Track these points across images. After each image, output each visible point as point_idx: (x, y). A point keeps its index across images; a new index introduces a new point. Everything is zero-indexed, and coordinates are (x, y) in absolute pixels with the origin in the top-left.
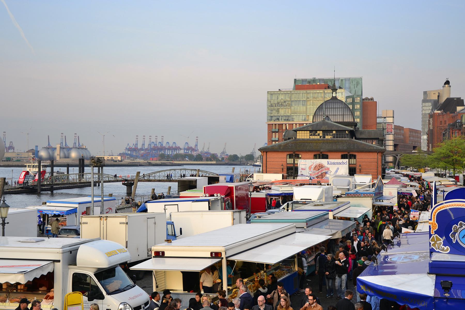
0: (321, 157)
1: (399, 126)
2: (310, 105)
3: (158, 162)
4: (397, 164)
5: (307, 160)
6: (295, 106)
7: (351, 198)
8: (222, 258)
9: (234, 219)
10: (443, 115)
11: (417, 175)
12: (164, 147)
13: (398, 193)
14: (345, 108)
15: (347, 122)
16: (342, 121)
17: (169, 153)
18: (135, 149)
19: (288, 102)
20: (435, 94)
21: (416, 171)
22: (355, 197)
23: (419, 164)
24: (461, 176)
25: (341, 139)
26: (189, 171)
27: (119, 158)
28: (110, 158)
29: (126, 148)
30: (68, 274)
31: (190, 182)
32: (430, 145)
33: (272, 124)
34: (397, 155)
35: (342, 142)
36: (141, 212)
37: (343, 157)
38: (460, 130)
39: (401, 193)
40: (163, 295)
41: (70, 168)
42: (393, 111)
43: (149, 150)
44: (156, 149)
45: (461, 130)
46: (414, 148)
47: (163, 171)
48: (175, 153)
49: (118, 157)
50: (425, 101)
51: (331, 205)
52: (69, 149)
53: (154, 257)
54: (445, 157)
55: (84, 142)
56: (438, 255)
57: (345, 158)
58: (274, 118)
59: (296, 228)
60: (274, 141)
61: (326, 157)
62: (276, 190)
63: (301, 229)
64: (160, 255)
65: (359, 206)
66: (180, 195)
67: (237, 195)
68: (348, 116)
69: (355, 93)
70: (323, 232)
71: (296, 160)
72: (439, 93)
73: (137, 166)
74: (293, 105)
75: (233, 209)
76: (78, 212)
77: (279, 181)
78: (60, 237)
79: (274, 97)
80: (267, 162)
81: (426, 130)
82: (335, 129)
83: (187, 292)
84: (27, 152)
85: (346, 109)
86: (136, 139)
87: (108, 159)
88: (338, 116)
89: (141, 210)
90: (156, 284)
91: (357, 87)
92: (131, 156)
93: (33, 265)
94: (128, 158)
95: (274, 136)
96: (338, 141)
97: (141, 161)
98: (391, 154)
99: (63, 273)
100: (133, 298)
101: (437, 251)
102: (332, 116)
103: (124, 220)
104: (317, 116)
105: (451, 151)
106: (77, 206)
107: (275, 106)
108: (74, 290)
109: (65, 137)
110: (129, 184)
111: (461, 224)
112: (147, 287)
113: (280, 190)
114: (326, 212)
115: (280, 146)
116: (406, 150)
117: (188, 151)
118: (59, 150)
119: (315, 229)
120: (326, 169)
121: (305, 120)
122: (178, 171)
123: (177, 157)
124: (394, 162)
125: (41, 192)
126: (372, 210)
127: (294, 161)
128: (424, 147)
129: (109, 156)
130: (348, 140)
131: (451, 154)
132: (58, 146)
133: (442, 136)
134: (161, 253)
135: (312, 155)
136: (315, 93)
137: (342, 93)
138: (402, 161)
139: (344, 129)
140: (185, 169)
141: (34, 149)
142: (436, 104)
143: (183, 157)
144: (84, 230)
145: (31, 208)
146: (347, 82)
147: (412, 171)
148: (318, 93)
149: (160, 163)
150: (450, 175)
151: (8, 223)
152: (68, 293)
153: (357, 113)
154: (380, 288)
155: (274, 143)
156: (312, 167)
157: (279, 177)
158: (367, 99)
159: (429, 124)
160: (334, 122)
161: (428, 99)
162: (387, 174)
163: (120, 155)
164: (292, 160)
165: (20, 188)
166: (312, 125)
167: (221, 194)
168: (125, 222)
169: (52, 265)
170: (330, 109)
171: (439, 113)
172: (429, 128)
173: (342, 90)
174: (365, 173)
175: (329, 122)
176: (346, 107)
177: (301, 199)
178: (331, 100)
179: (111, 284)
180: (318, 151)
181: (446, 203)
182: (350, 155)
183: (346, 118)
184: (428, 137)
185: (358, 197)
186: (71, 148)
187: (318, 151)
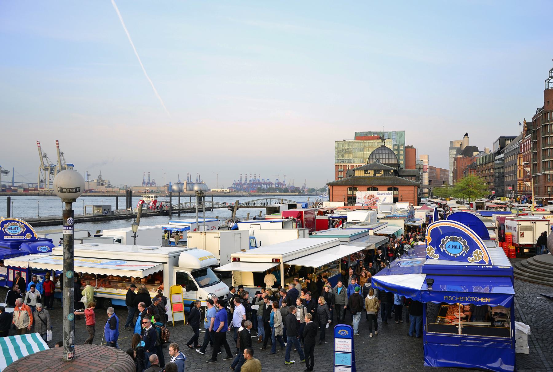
0: (373, 189)
2: (367, 151)
3: (256, 193)
4: (431, 195)
5: (363, 192)
6: (356, 152)
8: (281, 263)
9: (299, 235)
10: (464, 159)
11: (444, 202)
13: (426, 216)
14: (391, 153)
16: (389, 163)
17: (264, 187)
18: (240, 184)
19: (350, 149)
20: (458, 143)
22: (393, 219)
23: (445, 194)
24: (474, 203)
25: (387, 176)
26: (276, 200)
27: (228, 191)
28: (221, 190)
29: (233, 183)
31: (275, 208)
32: (455, 180)
33: (339, 165)
34: (431, 188)
35: (388, 178)
36: (234, 229)
37: (389, 189)
38: (476, 170)
39: (429, 216)
40: (238, 289)
42: (428, 155)
43: (249, 185)
44: (255, 184)
45: (477, 170)
46: (444, 183)
47: (258, 200)
48: (269, 187)
50: (451, 148)
52: (193, 184)
53: (232, 262)
54: (462, 190)
55: (203, 179)
57: (390, 191)
59: (341, 241)
60: (340, 178)
61: (376, 190)
62: (337, 214)
63: (345, 243)
64: (236, 260)
65: (394, 225)
66: (266, 218)
67: (306, 217)
68: (394, 159)
69: (400, 142)
70: (362, 244)
71: (354, 191)
72: (461, 143)
74: (354, 151)
75: (303, 227)
76: (191, 229)
77: (341, 207)
78: (178, 247)
79: (340, 146)
80: (333, 194)
81: (452, 169)
82: (383, 169)
83: (256, 287)
84: (164, 186)
85: (392, 154)
86: (284, 178)
88: (386, 159)
89: (234, 228)
90: (234, 281)
91: (401, 138)
92: (237, 189)
93: (149, 266)
94: (234, 190)
96: (385, 178)
97: (244, 193)
99: (169, 271)
100: (218, 291)
101: (431, 257)
103: (217, 235)
104: (370, 159)
105: (468, 186)
106: (190, 225)
107: (341, 152)
108: (177, 283)
109: (190, 175)
111: (447, 238)
112: (229, 284)
114: (367, 230)
115: (342, 181)
116: (438, 184)
117: (278, 186)
118: (186, 185)
119: (356, 242)
120: (376, 199)
121: (363, 162)
122: (268, 200)
123: (270, 190)
124: (429, 193)
125: (172, 215)
126: (404, 228)
128: (451, 183)
130: (392, 177)
131: (467, 187)
132: (185, 182)
133: (463, 174)
134: (237, 259)
135: (366, 188)
136: (370, 142)
137: (390, 142)
138: (434, 192)
139: (390, 169)
141: (169, 184)
142: (460, 151)
143: (274, 190)
144: (190, 241)
145: (159, 226)
146: (394, 134)
147: (440, 200)
148: (372, 142)
149: (258, 194)
150: (467, 203)
151: (138, 236)
152: (173, 285)
153: (402, 157)
154: (389, 285)
155: (340, 179)
156: (366, 197)
157: (342, 204)
158: (408, 147)
159: (454, 165)
160: (383, 164)
161: (453, 146)
162: (422, 202)
163: (229, 188)
164: (352, 191)
166: (366, 166)
168: (218, 237)
169: (162, 265)
170: (381, 154)
171: (461, 157)
172: (454, 168)
173: (390, 140)
175: (379, 163)
176: (392, 153)
177: (353, 221)
178: (381, 148)
179: (203, 280)
180: (370, 185)
181: (437, 223)
183: (392, 161)
184: (453, 175)
185: (395, 219)
186: (195, 184)
187: (370, 185)
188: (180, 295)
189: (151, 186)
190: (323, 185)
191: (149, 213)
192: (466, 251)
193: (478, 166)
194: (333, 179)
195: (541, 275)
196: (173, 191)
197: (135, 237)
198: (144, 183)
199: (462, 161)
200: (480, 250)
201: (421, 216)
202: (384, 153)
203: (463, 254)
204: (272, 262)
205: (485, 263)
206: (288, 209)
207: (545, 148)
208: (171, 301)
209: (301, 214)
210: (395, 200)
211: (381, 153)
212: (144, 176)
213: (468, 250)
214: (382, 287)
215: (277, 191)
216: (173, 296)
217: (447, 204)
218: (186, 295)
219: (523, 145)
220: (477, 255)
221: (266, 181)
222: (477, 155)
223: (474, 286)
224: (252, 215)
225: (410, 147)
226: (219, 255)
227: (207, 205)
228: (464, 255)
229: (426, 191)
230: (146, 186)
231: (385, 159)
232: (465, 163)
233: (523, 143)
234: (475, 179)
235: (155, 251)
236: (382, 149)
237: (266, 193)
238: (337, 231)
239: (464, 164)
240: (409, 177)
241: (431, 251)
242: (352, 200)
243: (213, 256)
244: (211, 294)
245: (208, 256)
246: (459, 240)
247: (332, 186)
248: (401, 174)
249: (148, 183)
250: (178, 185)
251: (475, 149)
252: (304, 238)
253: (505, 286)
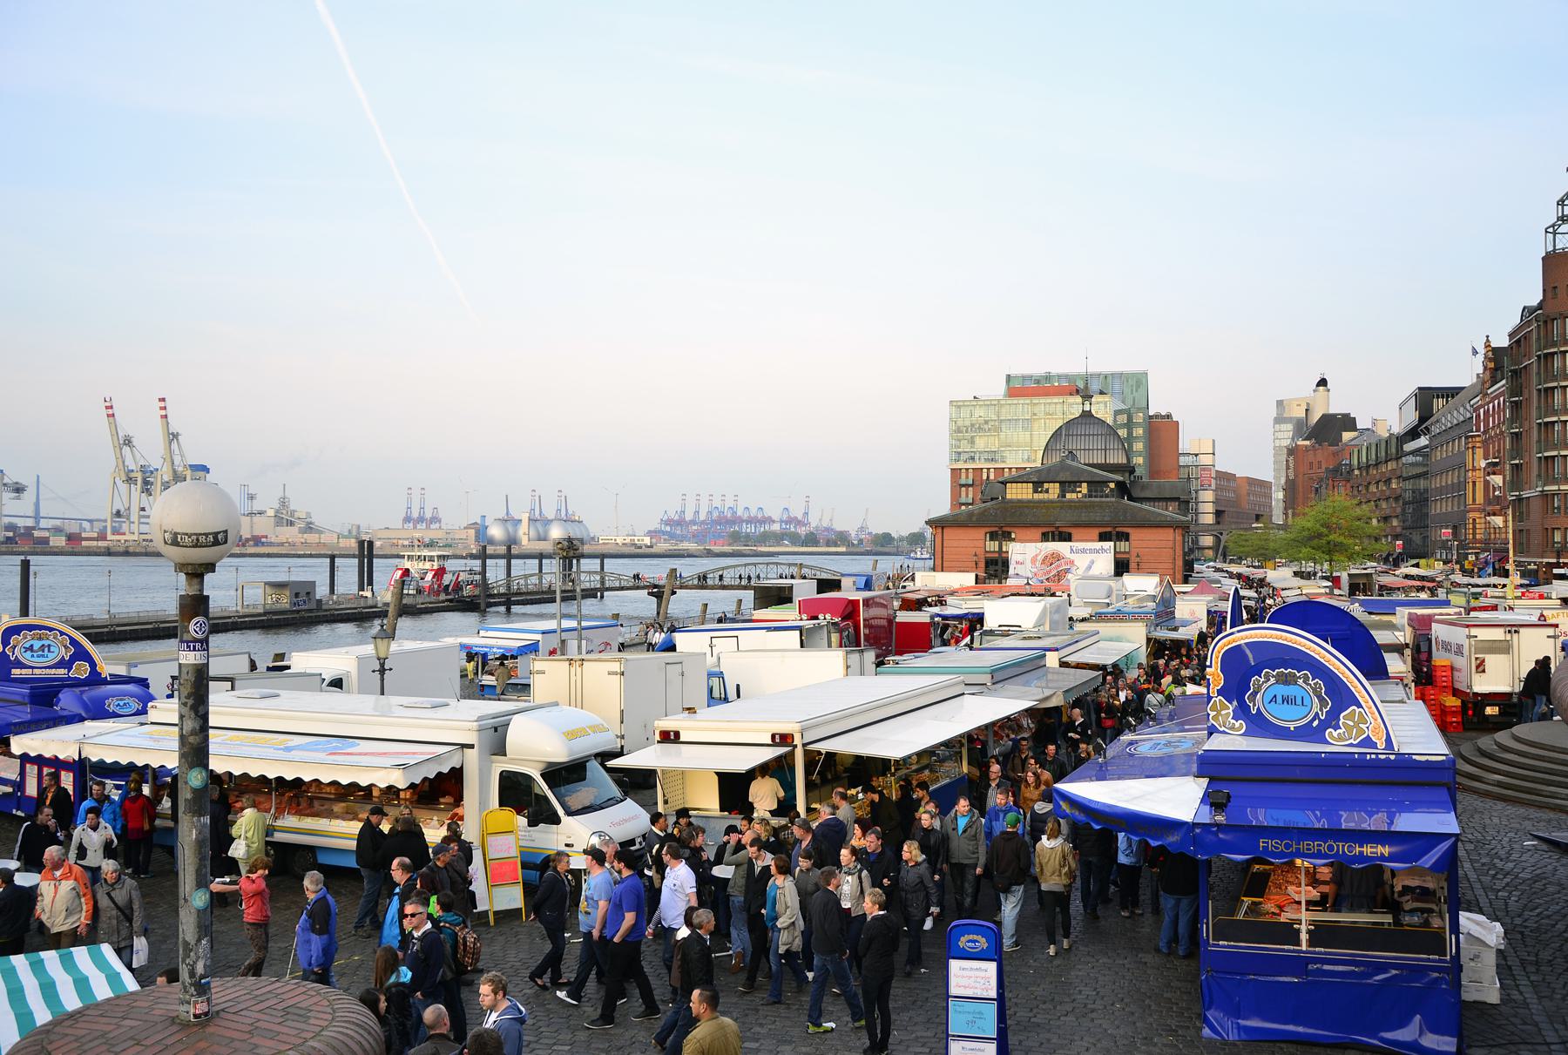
0: (1056, 537)
1: (1226, 473)
3: (727, 549)
4: (1222, 552)
7: (1119, 622)
8: (796, 746)
9: (848, 667)
11: (1258, 574)
12: (740, 517)
13: (1209, 612)
14: (1110, 435)
15: (1118, 464)
16: (1103, 462)
17: (748, 530)
18: (680, 523)
20: (1300, 405)
21: (1258, 567)
22: (1115, 620)
23: (1263, 551)
24: (1344, 576)
25: (1098, 499)
27: (647, 541)
29: (662, 520)
30: (490, 773)
31: (781, 589)
32: (1290, 512)
33: (960, 469)
34: (1221, 534)
35: (1100, 505)
37: (1104, 537)
39: (1215, 612)
40: (674, 819)
41: (544, 561)
42: (1214, 441)
43: (707, 524)
44: (723, 521)
45: (1351, 482)
46: (1258, 518)
47: (733, 569)
48: (762, 529)
49: (645, 538)
50: (1279, 420)
51: (1059, 637)
52: (547, 522)
53: (658, 742)
54: (1311, 538)
56: (1221, 738)
59: (966, 684)
60: (964, 504)
61: (1066, 537)
62: (955, 607)
63: (979, 688)
64: (669, 737)
65: (1118, 639)
66: (753, 618)
67: (867, 616)
68: (1116, 451)
69: (1134, 404)
70: (1025, 692)
71: (1004, 543)
72: (1308, 404)
73: (682, 556)
74: (1004, 429)
76: (540, 649)
78: (504, 700)
79: (965, 413)
81: (1283, 481)
82: (1087, 480)
83: (726, 813)
84: (465, 528)
85: (1112, 437)
87: (625, 542)
88: (1095, 451)
89: (663, 648)
90: (664, 796)
91: (1137, 391)
92: (672, 536)
93: (422, 754)
94: (665, 540)
95: (963, 494)
96: (1093, 505)
98: (1209, 530)
99: (480, 770)
100: (619, 824)
101: (1221, 729)
102: (1091, 452)
103: (616, 667)
104: (1050, 452)
105: (1328, 526)
106: (538, 637)
107: (967, 432)
109: (540, 497)
111: (1267, 674)
112: (648, 804)
113: (964, 606)
115: (971, 514)
119: (1010, 687)
120: (1066, 563)
121: (1028, 460)
122: (761, 566)
123: (765, 538)
124: (1215, 548)
125: (488, 610)
126: (1144, 647)
127: (1000, 547)
128: (1278, 519)
129: (627, 535)
130: (1112, 502)
131: (1324, 530)
132: (525, 517)
133: (1313, 492)
134: (672, 733)
135: (1038, 533)
136: (1050, 403)
137: (1105, 403)
138: (1231, 545)
139: (1105, 479)
140: (777, 564)
141: (479, 522)
142: (1301, 427)
143: (778, 538)
144: (538, 683)
145: (450, 641)
146: (1117, 381)
147: (1248, 567)
149: (731, 551)
150: (1324, 574)
151: (391, 669)
152: (491, 809)
153: (1139, 446)
154: (1102, 808)
155: (963, 508)
156: (1039, 558)
157: (968, 579)
158: (1157, 416)
159: (1288, 468)
160: (1085, 464)
162: (1197, 573)
164: (997, 543)
165: (447, 600)
166: (1037, 471)
167: (833, 616)
168: (619, 671)
171: (1306, 446)
172: (1287, 476)
173: (1106, 398)
174: (1149, 570)
175: (1074, 464)
176: (1112, 433)
177: (1000, 626)
178: (1080, 419)
179: (574, 795)
180: (1050, 525)
181: (1239, 631)
182: (1118, 532)
183: (1112, 456)
184: (1285, 496)
185: (1121, 620)
186: (552, 521)
187: (1050, 525)
188: (511, 838)
189: (428, 527)
190: (916, 524)
191: (422, 604)
192: (1320, 713)
193: (1356, 472)
194: (943, 508)
196: (491, 542)
197: (382, 671)
198: (407, 519)
199: (1310, 457)
200: (1361, 710)
201: (1193, 613)
202: (1089, 435)
203: (1314, 719)
204: (770, 742)
205: (1374, 745)
206: (818, 593)
208: (484, 855)
209: (853, 606)
210: (1121, 568)
211: (1079, 433)
212: (409, 500)
213: (1328, 709)
214: (1083, 812)
215: (786, 542)
216: (491, 840)
217: (1268, 580)
218: (528, 838)
219: (1482, 411)
220: (1352, 724)
221: (753, 512)
222: (1352, 440)
223: (1345, 811)
224: (715, 609)
225: (1161, 416)
226: (622, 722)
228: (1315, 723)
229: (1207, 541)
230: (415, 528)
231: (1093, 450)
232: (1320, 462)
234: (1346, 508)
235: (440, 713)
236: (1088, 422)
237: (755, 548)
238: (955, 656)
239: (1315, 466)
240: (1159, 502)
241: (1223, 712)
242: (999, 567)
243: (605, 725)
244: (600, 834)
245: (590, 727)
246: (1301, 681)
247: (943, 528)
248: (1136, 493)
249: (421, 519)
250: (504, 525)
251: (1348, 422)
252: (862, 674)
253: (1431, 810)
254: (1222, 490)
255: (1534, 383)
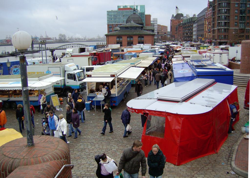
1: (159, 25)
58: (117, 22)
110: (52, 51)
195: (243, 83)
207: (219, 15)
219: (207, 13)
227: (35, 49)
232: (177, 23)
233: (207, 13)
247: (108, 36)
251: (182, 15)
254: (158, 28)
255: (217, 10)
